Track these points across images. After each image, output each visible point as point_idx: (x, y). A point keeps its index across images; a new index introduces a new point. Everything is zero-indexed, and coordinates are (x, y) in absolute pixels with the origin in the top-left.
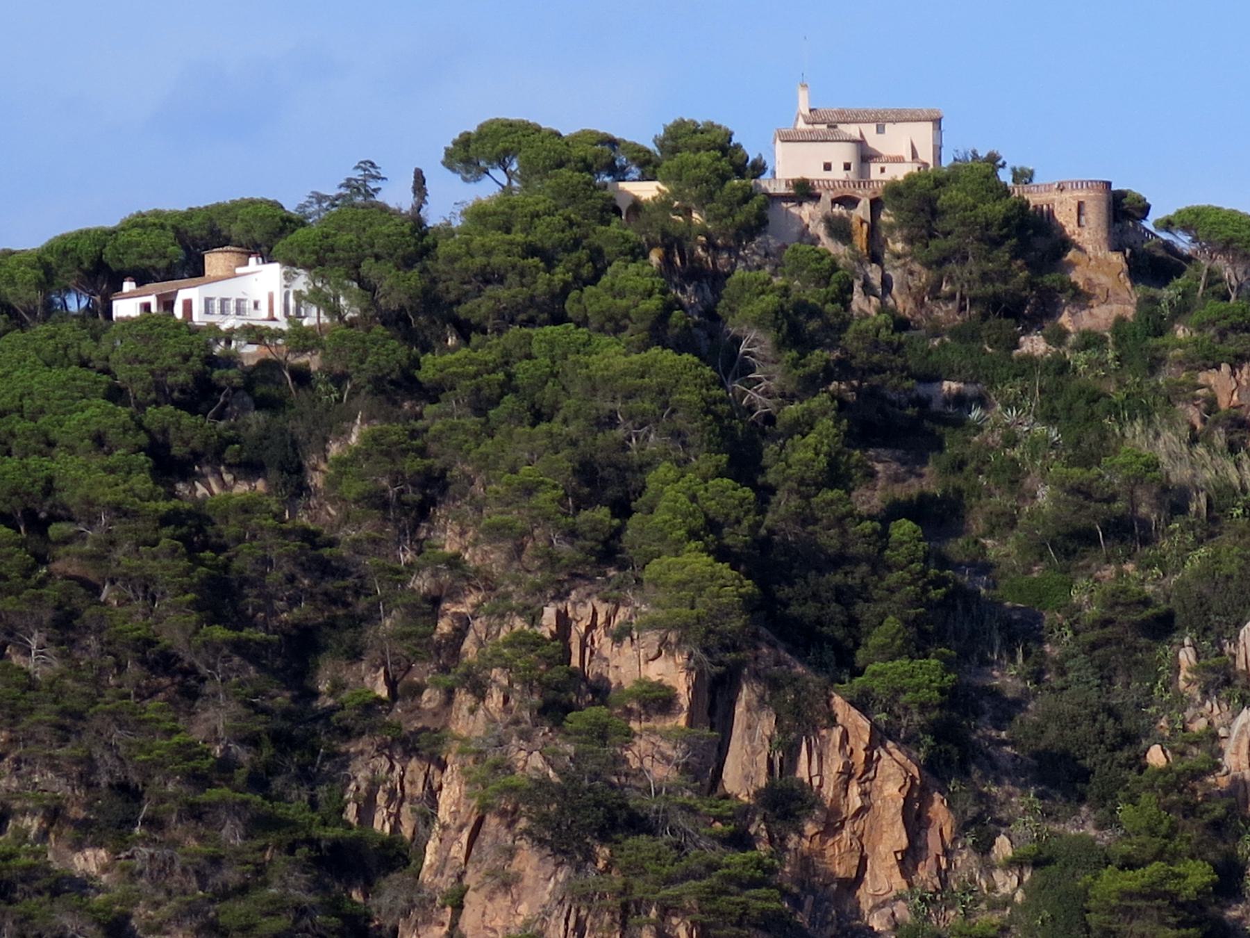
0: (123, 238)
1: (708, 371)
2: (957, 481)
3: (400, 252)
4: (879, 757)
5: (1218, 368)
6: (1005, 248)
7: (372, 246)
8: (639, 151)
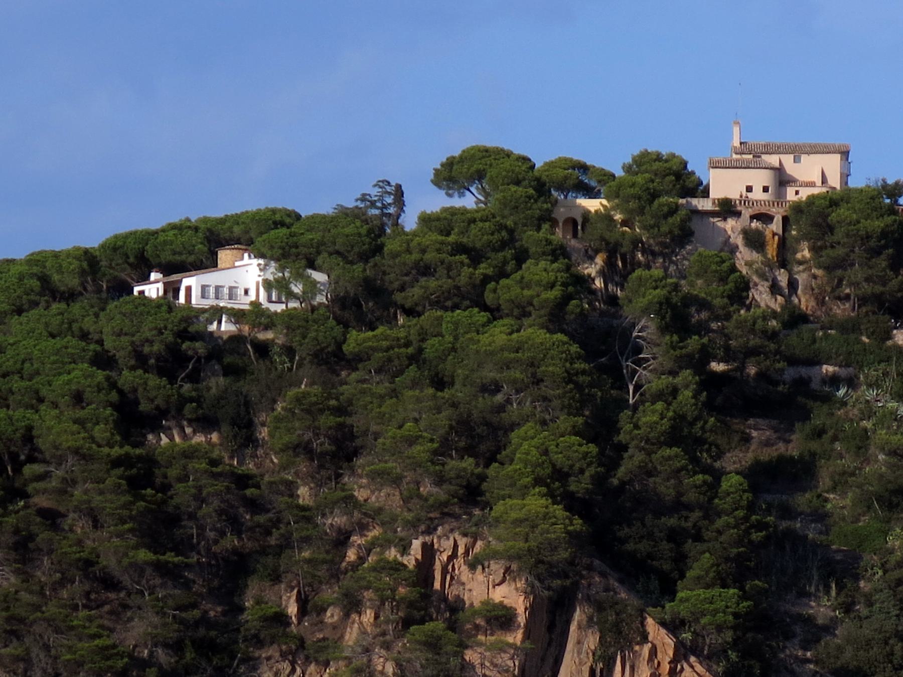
0: (161, 238)
1: (575, 348)
2: (814, 446)
3: (356, 249)
6: (883, 257)
7: (335, 243)
8: (605, 175)
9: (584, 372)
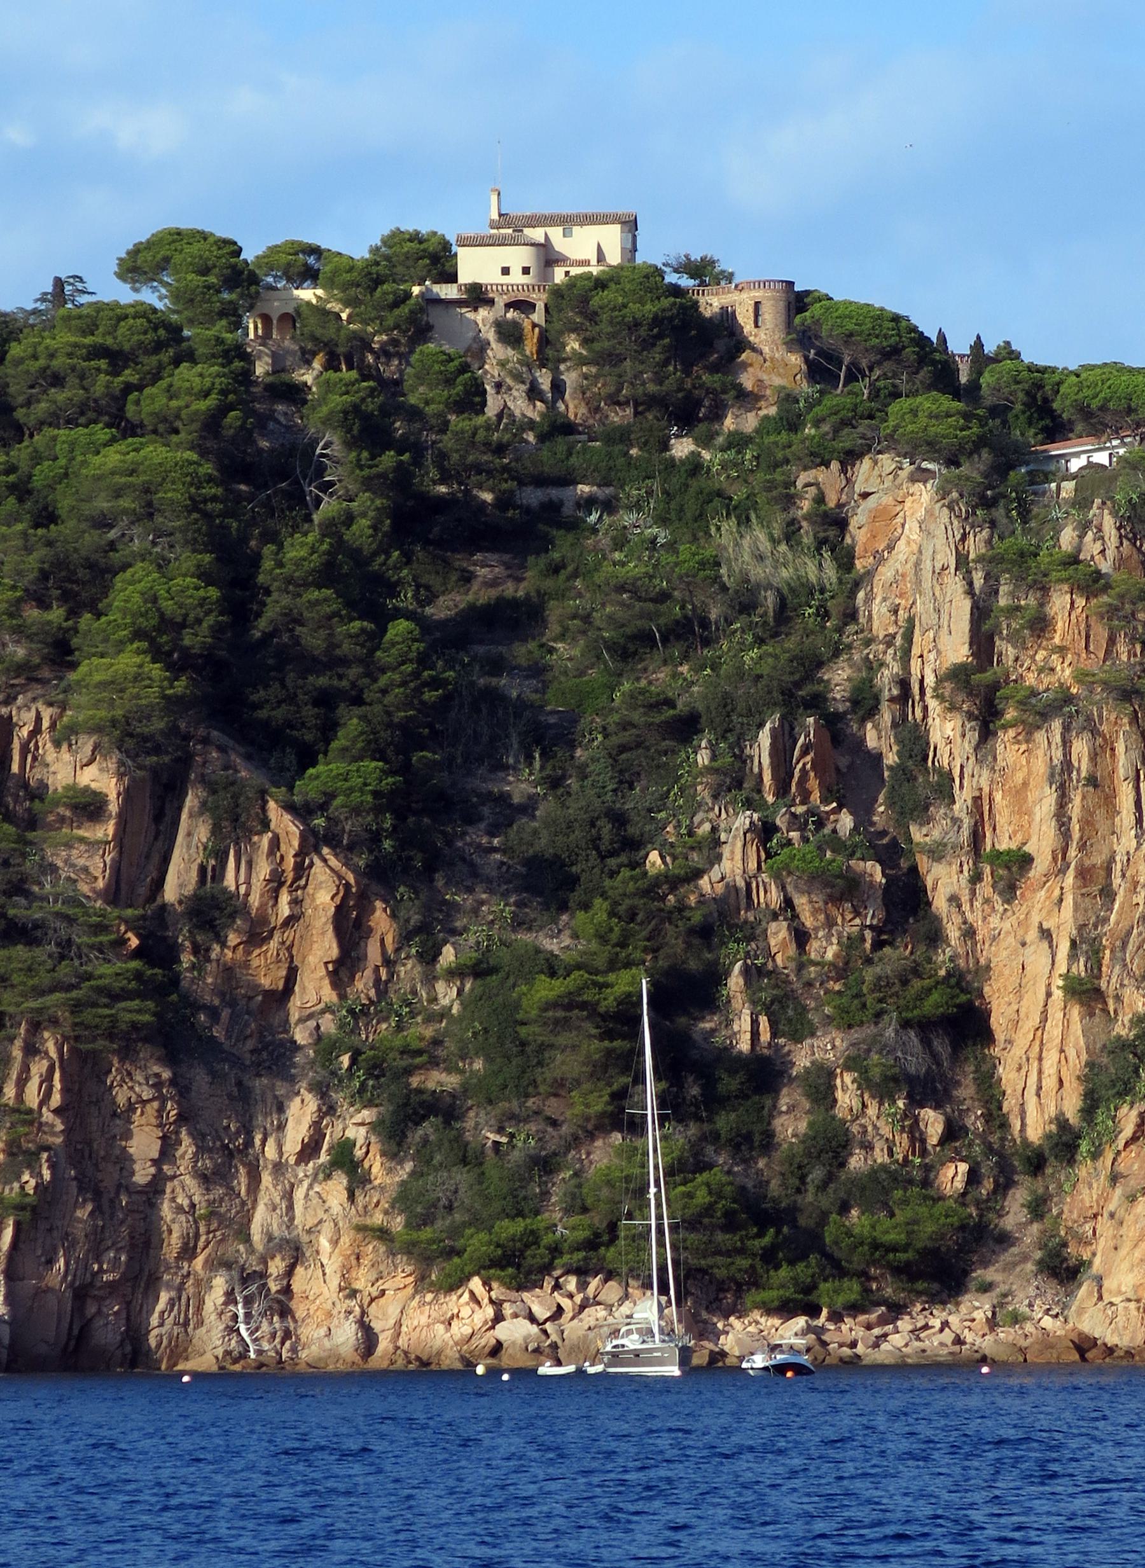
2: (548, 584)
4: (312, 864)
5: (828, 466)
6: (658, 349)
9: (214, 499)
